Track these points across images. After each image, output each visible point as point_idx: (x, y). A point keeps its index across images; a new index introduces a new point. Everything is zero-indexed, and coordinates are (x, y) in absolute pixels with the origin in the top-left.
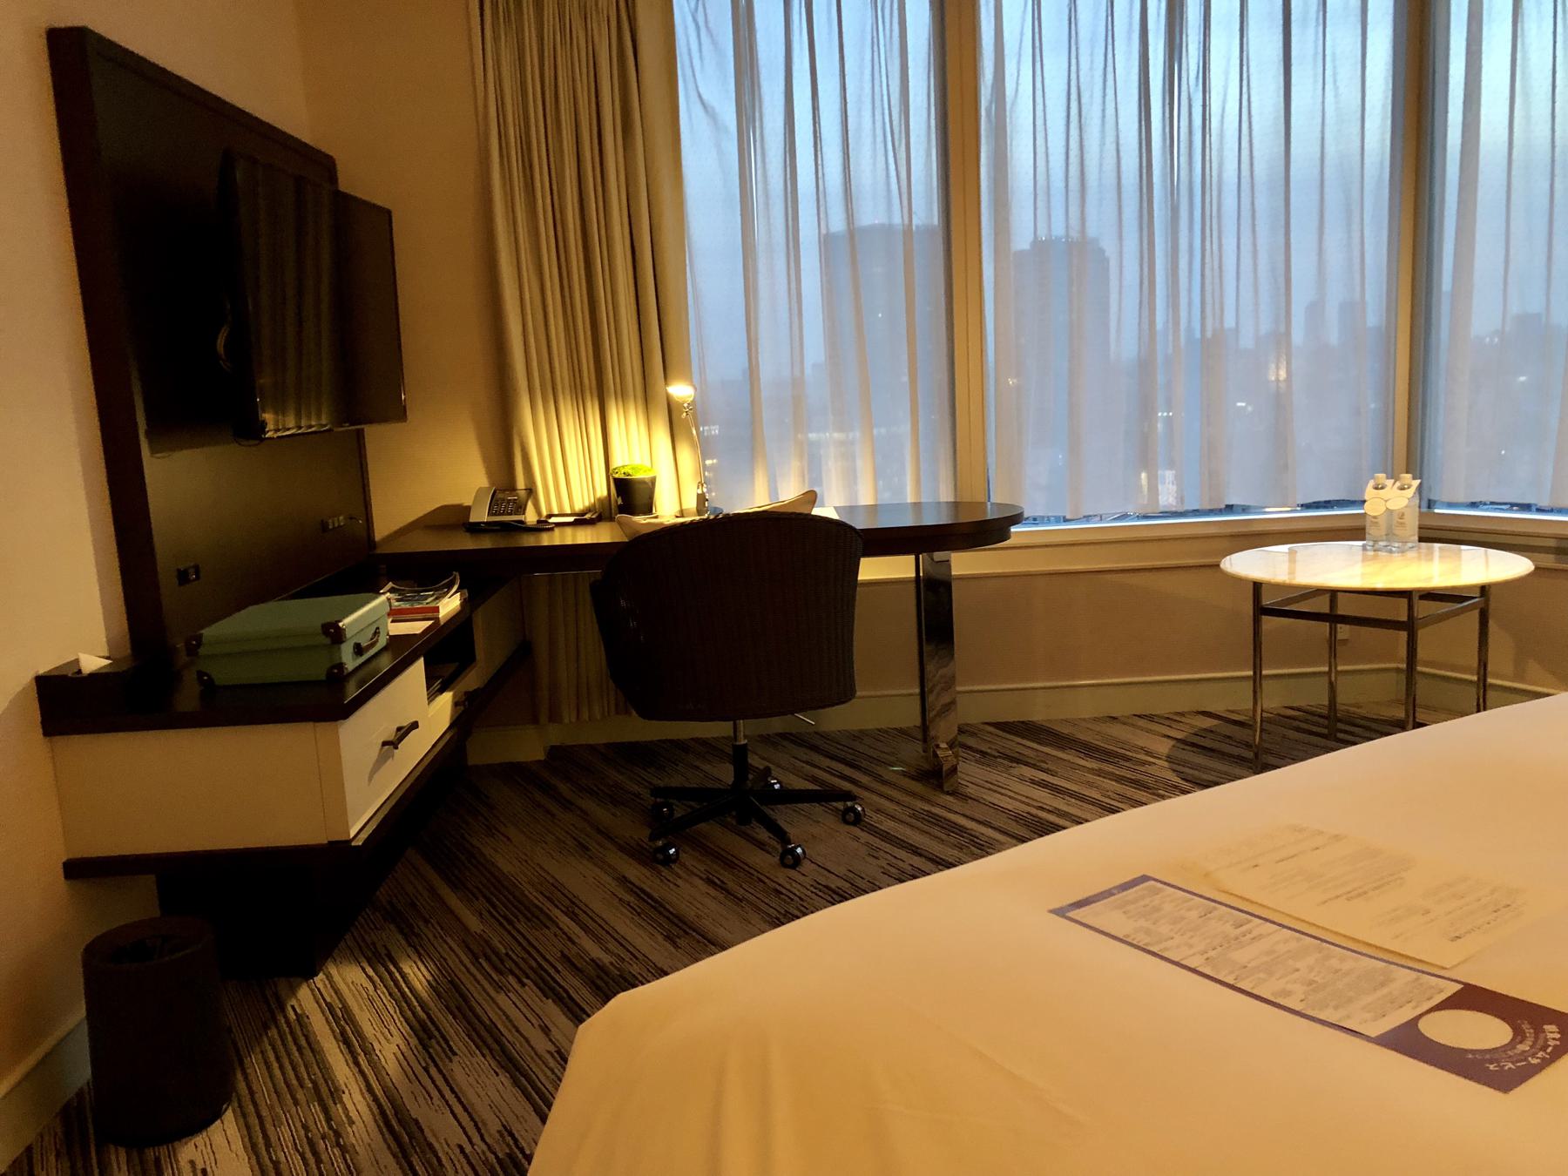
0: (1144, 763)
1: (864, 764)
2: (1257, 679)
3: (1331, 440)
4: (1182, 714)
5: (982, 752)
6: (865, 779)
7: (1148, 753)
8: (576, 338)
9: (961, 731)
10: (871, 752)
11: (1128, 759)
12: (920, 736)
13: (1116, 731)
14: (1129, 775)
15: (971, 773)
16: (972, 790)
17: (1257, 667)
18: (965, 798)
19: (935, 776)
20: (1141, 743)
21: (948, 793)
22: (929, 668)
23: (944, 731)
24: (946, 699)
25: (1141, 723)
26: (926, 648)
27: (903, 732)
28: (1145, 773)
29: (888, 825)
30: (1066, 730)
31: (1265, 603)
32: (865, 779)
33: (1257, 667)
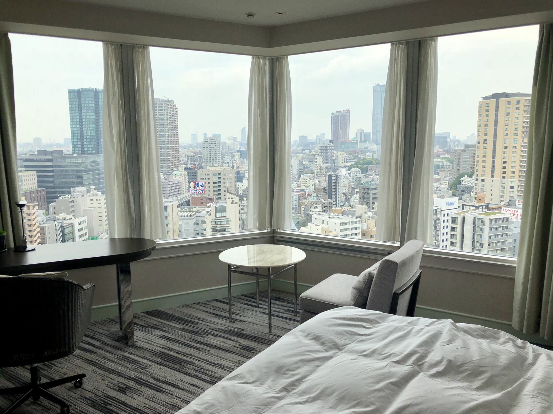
0: (198, 323)
1: (97, 336)
2: (230, 287)
3: (238, 214)
4: (208, 301)
5: (141, 326)
6: (98, 344)
7: (199, 319)
8: (150, 207)
9: (134, 317)
10: (100, 331)
11: (192, 322)
12: (118, 320)
13: (187, 311)
14: (191, 329)
15: (138, 335)
16: (139, 344)
17: (230, 283)
18: (138, 348)
19: (125, 339)
20: (197, 315)
21: (130, 346)
22: (122, 287)
23: (128, 317)
24: (128, 303)
25: (196, 306)
26: (121, 277)
27: (112, 320)
28: (197, 328)
29: (109, 365)
30: (170, 312)
31: (232, 269)
32: (98, 344)
33: (230, 283)
